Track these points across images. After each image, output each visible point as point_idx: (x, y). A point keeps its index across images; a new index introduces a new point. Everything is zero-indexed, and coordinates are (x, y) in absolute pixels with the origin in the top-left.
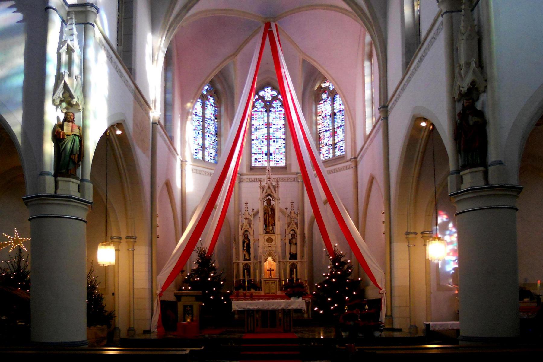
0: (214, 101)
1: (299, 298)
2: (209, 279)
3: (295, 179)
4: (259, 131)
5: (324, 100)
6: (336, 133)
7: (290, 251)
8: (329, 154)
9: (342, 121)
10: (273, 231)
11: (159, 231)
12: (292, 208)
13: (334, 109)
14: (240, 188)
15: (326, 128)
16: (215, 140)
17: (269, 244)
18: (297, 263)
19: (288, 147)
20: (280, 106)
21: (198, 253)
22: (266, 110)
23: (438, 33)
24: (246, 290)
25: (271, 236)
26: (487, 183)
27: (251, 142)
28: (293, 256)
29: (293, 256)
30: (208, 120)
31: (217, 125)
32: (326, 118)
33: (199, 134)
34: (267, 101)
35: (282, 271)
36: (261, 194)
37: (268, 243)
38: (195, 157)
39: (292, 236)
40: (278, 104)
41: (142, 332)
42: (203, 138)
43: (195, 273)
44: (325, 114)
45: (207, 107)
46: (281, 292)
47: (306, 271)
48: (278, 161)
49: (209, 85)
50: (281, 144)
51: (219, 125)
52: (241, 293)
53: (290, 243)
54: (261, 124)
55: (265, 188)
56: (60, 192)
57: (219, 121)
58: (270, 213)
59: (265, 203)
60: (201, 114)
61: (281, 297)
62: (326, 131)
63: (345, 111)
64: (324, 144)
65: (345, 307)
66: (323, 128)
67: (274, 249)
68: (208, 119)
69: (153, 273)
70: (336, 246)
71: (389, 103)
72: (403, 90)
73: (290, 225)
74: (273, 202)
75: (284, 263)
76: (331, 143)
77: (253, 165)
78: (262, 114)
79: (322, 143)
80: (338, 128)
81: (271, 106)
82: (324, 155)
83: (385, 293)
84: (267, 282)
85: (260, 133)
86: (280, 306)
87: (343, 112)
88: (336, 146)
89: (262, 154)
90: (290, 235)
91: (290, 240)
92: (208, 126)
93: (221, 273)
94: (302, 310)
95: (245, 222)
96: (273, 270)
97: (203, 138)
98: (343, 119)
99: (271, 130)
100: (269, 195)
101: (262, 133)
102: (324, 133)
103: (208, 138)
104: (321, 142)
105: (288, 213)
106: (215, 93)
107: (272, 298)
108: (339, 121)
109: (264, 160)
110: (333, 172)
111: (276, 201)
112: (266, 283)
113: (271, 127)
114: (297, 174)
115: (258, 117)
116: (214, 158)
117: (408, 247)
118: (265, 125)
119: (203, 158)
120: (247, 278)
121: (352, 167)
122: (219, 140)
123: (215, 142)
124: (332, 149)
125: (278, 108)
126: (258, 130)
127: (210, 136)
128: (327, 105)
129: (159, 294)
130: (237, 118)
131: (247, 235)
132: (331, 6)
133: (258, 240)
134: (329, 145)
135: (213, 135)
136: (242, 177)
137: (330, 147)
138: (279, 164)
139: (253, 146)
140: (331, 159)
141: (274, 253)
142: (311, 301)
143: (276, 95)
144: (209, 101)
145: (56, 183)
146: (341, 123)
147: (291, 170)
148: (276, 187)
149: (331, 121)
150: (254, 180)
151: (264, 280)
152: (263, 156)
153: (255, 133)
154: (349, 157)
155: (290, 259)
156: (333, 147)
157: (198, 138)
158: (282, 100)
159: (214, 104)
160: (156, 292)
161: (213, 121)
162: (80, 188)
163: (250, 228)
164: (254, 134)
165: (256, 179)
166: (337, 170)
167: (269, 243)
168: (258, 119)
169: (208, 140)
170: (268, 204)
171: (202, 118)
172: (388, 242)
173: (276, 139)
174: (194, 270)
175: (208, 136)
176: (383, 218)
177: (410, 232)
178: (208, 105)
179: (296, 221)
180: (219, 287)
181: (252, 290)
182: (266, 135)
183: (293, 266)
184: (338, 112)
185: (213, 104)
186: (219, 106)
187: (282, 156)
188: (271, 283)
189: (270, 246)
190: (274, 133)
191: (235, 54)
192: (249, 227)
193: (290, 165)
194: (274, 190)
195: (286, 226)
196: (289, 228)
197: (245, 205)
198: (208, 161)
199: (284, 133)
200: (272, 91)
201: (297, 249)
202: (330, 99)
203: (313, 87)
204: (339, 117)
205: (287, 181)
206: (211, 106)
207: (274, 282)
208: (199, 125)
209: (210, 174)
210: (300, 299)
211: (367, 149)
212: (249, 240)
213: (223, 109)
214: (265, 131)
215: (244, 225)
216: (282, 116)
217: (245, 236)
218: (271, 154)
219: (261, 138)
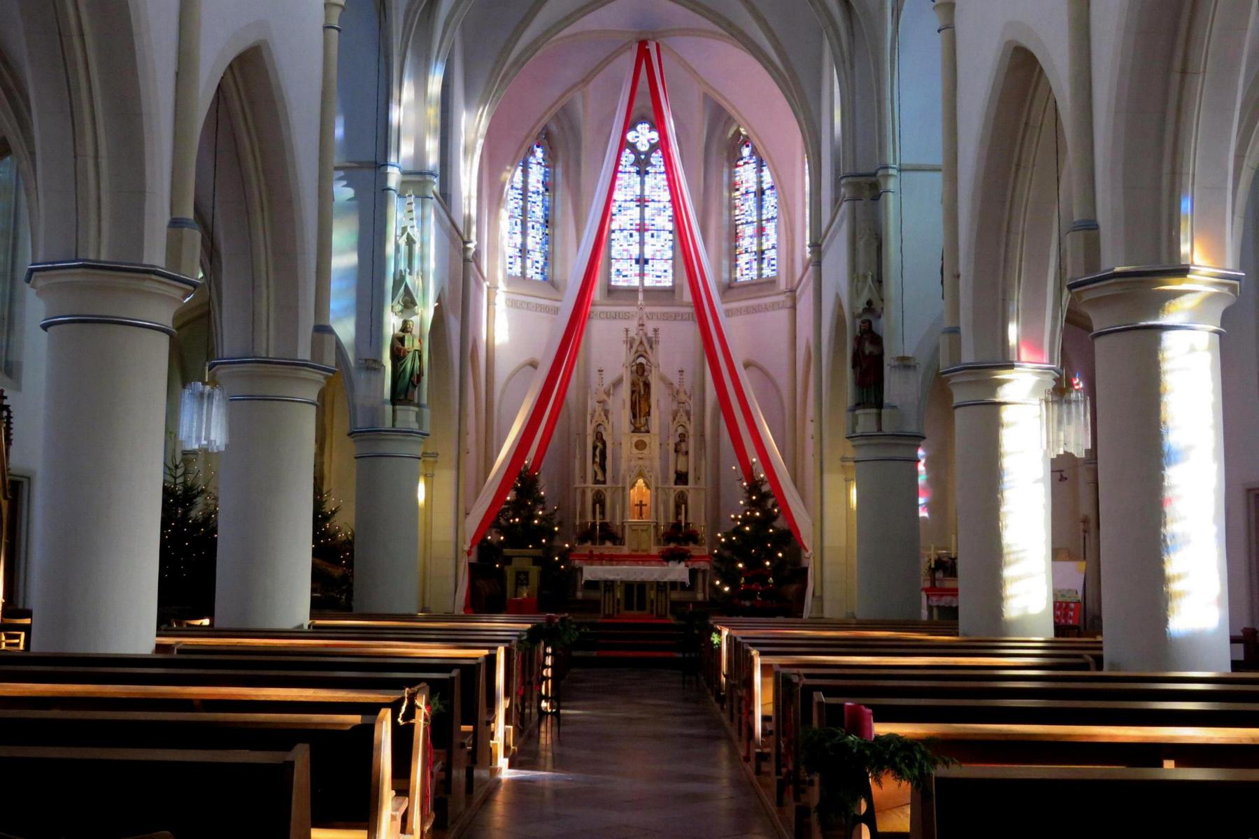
0: (544, 155)
1: (679, 562)
2: (536, 522)
4: (625, 213)
10: (648, 426)
12: (681, 381)
13: (762, 182)
16: (543, 233)
17: (639, 454)
18: (688, 490)
22: (638, 169)
23: (840, 226)
25: (643, 437)
26: (880, 429)
29: (682, 478)
30: (533, 195)
31: (549, 202)
32: (747, 197)
33: (516, 225)
35: (661, 508)
37: (638, 451)
38: (509, 271)
39: (679, 436)
42: (524, 233)
44: (747, 188)
48: (660, 277)
53: (676, 451)
56: (399, 425)
57: (552, 194)
60: (519, 185)
62: (747, 223)
63: (780, 190)
66: (742, 216)
67: (647, 463)
68: (533, 193)
69: (461, 512)
71: (823, 240)
77: (613, 283)
79: (739, 246)
80: (768, 220)
81: (648, 163)
82: (741, 270)
84: (634, 528)
85: (625, 218)
89: (629, 261)
91: (677, 445)
92: (532, 207)
93: (555, 510)
96: (646, 505)
97: (524, 233)
99: (648, 212)
100: (641, 356)
102: (744, 226)
104: (737, 244)
107: (642, 561)
109: (632, 273)
110: (755, 310)
112: (633, 530)
113: (647, 206)
116: (542, 269)
118: (636, 201)
119: (523, 274)
122: (552, 232)
126: (623, 212)
127: (535, 227)
130: (593, 221)
133: (621, 444)
134: (751, 252)
135: (540, 223)
141: (648, 472)
142: (709, 568)
144: (535, 156)
145: (394, 411)
152: (631, 265)
155: (676, 483)
162: (419, 418)
165: (617, 314)
167: (640, 450)
168: (623, 189)
172: (819, 472)
173: (657, 230)
181: (608, 544)
182: (638, 222)
184: (769, 189)
188: (642, 530)
190: (653, 218)
192: (604, 418)
195: (671, 418)
201: (688, 465)
203: (725, 132)
204: (770, 199)
205: (675, 319)
206: (539, 166)
207: (645, 528)
208: (516, 208)
209: (535, 306)
210: (682, 565)
212: (604, 444)
213: (559, 170)
215: (597, 414)
218: (646, 262)
219: (629, 227)
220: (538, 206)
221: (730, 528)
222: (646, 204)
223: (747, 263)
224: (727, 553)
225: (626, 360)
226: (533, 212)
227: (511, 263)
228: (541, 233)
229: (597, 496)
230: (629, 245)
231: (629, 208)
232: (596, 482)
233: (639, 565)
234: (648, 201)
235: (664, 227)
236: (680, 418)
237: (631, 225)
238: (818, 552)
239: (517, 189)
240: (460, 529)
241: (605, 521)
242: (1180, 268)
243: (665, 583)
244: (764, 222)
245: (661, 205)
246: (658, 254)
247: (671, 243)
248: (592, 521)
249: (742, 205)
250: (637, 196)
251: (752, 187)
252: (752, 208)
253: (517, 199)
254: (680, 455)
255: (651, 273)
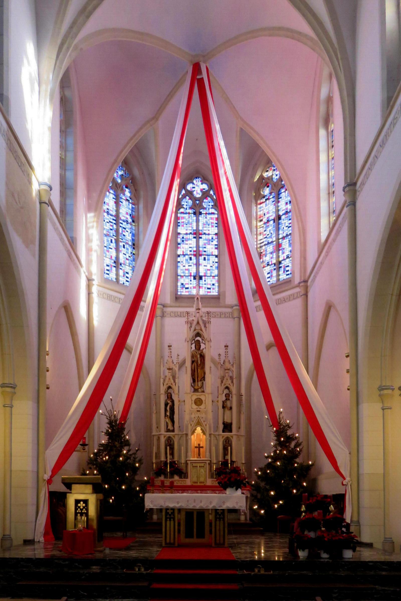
0: (131, 195)
1: (237, 489)
3: (229, 315)
4: (187, 243)
5: (266, 198)
6: (281, 247)
7: (224, 419)
8: (272, 278)
9: (289, 227)
10: (203, 389)
11: (49, 377)
12: (226, 353)
13: (278, 210)
14: (162, 326)
15: (268, 240)
16: (131, 253)
17: (197, 408)
18: (232, 437)
19: (221, 266)
20: (212, 205)
21: (108, 419)
22: (194, 211)
23: (342, 224)
24: (169, 477)
25: (200, 395)
27: (176, 259)
28: (227, 427)
29: (227, 427)
30: (124, 223)
32: (268, 224)
33: (111, 242)
34: (196, 199)
35: (213, 449)
36: (188, 331)
38: (106, 276)
39: (226, 396)
40: (210, 204)
41: (22, 542)
43: (105, 448)
44: (268, 218)
45: (122, 202)
46: (212, 481)
47: (243, 449)
49: (124, 169)
50: (213, 264)
51: (137, 232)
52: (177, 482)
53: (224, 407)
54: (188, 233)
55: (193, 323)
57: (137, 224)
58: (199, 361)
59: (193, 346)
60: (114, 213)
61: (212, 489)
62: (269, 243)
64: (266, 262)
65: (301, 507)
66: (265, 240)
67: (203, 415)
68: (124, 221)
70: (281, 412)
72: (382, 146)
73: (224, 379)
74: (203, 346)
75: (216, 437)
76: (274, 261)
77: (179, 293)
78: (190, 217)
80: (283, 238)
83: (351, 485)
84: (194, 465)
86: (211, 503)
87: (290, 214)
88: (281, 266)
89: (189, 277)
90: (224, 395)
92: (122, 231)
94: (240, 510)
95: (167, 373)
96: (202, 447)
97: (117, 249)
98: (290, 225)
99: (201, 242)
100: (198, 335)
101: (191, 246)
102: (266, 246)
103: (124, 249)
105: (221, 362)
106: (131, 182)
108: (285, 228)
109: (192, 286)
111: (207, 343)
112: (193, 467)
113: (201, 238)
114: (232, 307)
115: (185, 223)
117: (382, 410)
119: (117, 279)
120: (170, 459)
121: (301, 296)
122: (137, 253)
123: (131, 256)
124: (275, 271)
125: (210, 209)
127: (125, 246)
128: (270, 205)
129: (47, 480)
131: (170, 393)
132: (280, 29)
133: (184, 401)
134: (272, 264)
135: (129, 245)
136: (165, 309)
137: (273, 267)
138: (210, 292)
139: (179, 264)
140: (274, 285)
143: (208, 189)
144: (124, 195)
146: (287, 231)
147: (225, 302)
148: (207, 322)
149: (274, 228)
150: (180, 315)
151: (191, 463)
152: (191, 281)
153: (182, 246)
154: (297, 280)
155: (223, 431)
156: (277, 268)
157: (110, 248)
158: (215, 197)
159: (130, 199)
160: (43, 477)
161: (129, 225)
163: (175, 383)
164: (180, 248)
166: (282, 301)
168: (185, 225)
169: (122, 252)
170: (197, 348)
171: (115, 219)
173: (208, 255)
174: (102, 445)
175: (122, 247)
176: (347, 364)
177: (384, 386)
178: (123, 200)
179: (231, 375)
180: (135, 470)
181: (176, 478)
183: (227, 442)
185: (129, 199)
186: (136, 202)
187: (214, 281)
188: (200, 467)
189: (199, 411)
190: (205, 246)
191: (155, 118)
192: (172, 381)
193: (225, 292)
194: (204, 327)
195: (219, 381)
196: (223, 384)
197: (168, 348)
198: (124, 283)
199: (216, 247)
200: (202, 184)
202: (274, 196)
203: (253, 176)
204: (285, 222)
207: (202, 465)
208: (111, 229)
210: (239, 491)
211: (322, 263)
212: (173, 402)
213: (141, 206)
214: (193, 242)
215: (167, 379)
216: (215, 222)
217: (167, 396)
219: (189, 253)
220: (127, 231)
221: (262, 465)
222: (200, 236)
223: (268, 273)
224: (262, 484)
225: (188, 336)
226: (124, 235)
227: (108, 270)
228: (129, 253)
229: (168, 441)
230: (189, 266)
231: (189, 239)
232: (168, 430)
233: (198, 493)
234: (201, 234)
235: (212, 252)
236: (226, 381)
237: (191, 251)
238: (355, 480)
239: (112, 215)
240: (41, 458)
241: (174, 460)
242: (183, 508)
243: (223, 510)
244: (280, 240)
245: (210, 237)
246: (209, 272)
247: (216, 264)
248: (165, 460)
249: (265, 231)
250: (194, 230)
251: (272, 216)
252: (272, 232)
253: (112, 223)
254: (226, 409)
255: (204, 286)
